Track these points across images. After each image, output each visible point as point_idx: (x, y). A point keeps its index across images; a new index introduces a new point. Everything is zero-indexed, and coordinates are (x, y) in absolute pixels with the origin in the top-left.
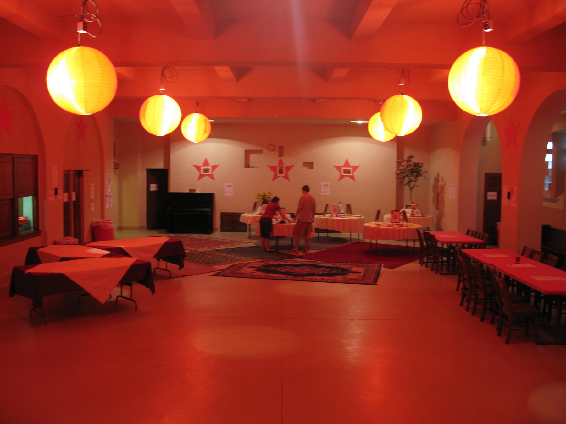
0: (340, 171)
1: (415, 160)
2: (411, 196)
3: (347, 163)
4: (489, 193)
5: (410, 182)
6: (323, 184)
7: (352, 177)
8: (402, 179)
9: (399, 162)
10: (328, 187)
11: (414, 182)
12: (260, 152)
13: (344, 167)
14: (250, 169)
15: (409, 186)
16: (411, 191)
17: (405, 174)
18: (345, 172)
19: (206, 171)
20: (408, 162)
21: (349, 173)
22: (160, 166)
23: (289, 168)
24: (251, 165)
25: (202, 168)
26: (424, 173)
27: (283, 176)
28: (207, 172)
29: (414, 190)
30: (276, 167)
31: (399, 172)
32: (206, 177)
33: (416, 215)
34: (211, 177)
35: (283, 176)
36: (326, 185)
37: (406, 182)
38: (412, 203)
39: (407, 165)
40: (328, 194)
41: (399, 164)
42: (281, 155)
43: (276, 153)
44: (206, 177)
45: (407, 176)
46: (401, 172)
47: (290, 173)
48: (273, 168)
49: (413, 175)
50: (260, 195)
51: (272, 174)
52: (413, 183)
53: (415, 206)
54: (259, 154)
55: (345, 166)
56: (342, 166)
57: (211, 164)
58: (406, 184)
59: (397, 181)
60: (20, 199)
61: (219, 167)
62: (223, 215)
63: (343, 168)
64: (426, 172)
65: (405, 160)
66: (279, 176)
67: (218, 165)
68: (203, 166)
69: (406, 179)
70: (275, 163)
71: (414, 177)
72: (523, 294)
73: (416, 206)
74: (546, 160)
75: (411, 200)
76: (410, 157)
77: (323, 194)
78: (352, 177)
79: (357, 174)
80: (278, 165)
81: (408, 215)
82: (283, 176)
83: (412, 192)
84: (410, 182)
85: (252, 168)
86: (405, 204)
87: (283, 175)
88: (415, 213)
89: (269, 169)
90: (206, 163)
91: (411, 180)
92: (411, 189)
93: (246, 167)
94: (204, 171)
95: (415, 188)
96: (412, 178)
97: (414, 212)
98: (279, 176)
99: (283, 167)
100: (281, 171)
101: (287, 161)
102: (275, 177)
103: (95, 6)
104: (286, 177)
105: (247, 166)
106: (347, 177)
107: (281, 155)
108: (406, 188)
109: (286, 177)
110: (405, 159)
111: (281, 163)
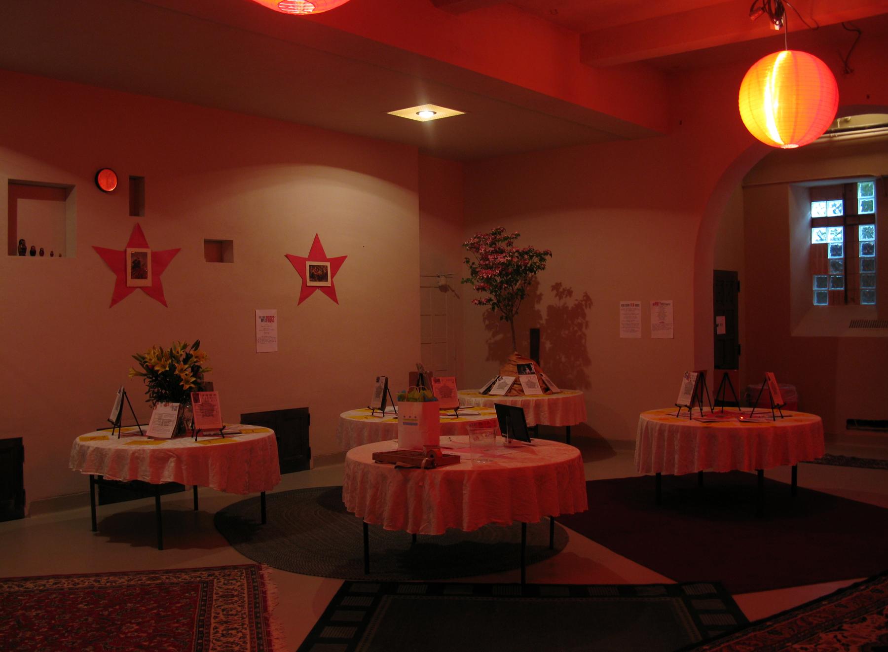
4: (718, 318)
6: (260, 313)
7: (330, 292)
10: (274, 325)
12: (62, 193)
13: (309, 259)
14: (28, 257)
18: (313, 277)
21: (324, 277)
23: (162, 260)
27: (144, 289)
32: (138, 295)
33: (527, 391)
35: (144, 289)
36: (270, 319)
40: (273, 347)
44: (318, 291)
47: (166, 278)
48: (111, 258)
51: (111, 278)
56: (306, 255)
63: (308, 263)
68: (310, 258)
70: (119, 242)
72: (53, 604)
77: (261, 348)
78: (330, 292)
79: (342, 281)
80: (130, 245)
82: (144, 289)
85: (33, 253)
87: (148, 282)
89: (97, 257)
93: (11, 252)
99: (145, 254)
100: (139, 271)
102: (121, 292)
104: (156, 292)
105: (18, 248)
107: (135, 210)
109: (156, 292)
111: (138, 237)
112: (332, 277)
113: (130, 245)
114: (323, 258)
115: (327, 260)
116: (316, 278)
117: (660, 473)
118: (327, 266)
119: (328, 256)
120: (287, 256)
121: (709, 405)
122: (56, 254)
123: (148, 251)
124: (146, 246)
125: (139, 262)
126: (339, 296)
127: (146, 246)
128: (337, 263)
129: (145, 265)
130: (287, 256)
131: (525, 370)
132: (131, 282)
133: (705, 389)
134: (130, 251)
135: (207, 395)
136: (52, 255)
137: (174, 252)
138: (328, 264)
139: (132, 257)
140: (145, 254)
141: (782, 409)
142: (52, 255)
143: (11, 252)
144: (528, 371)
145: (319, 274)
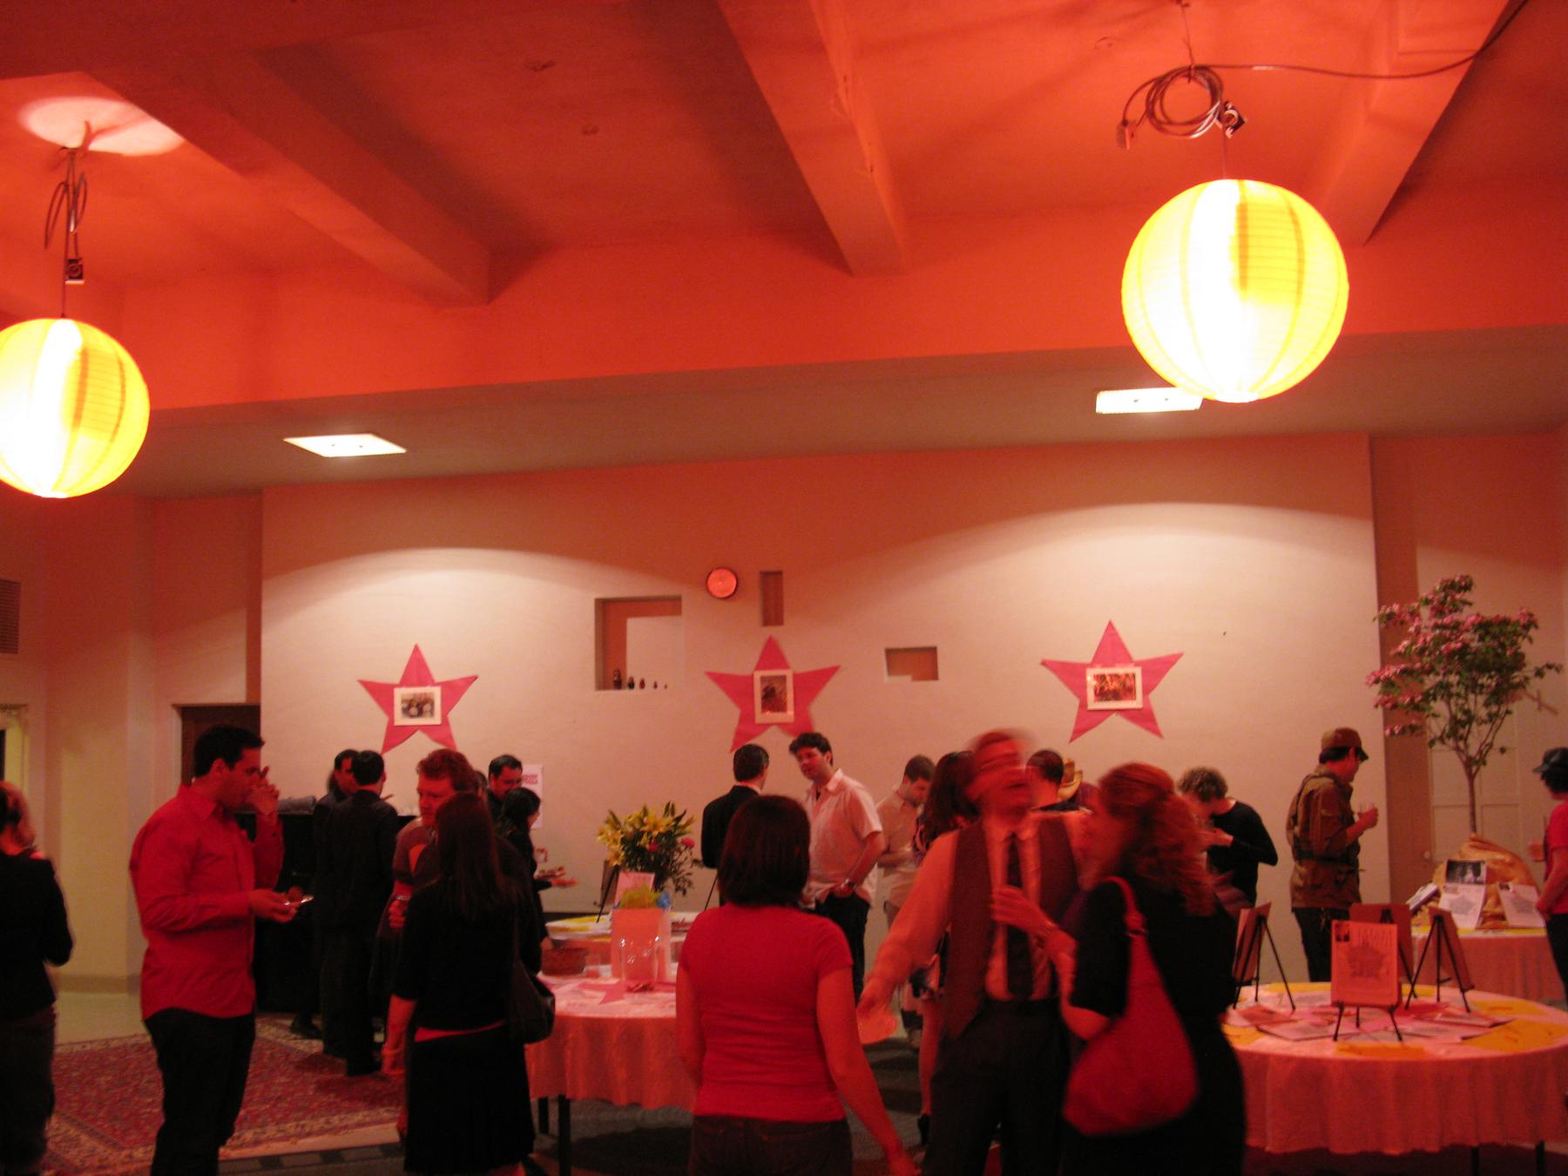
0: (1078, 688)
1: (1484, 603)
2: (1473, 805)
3: (1112, 646)
5: (1458, 728)
8: (1416, 707)
9: (1390, 616)
11: (1485, 728)
12: (666, 606)
14: (626, 692)
15: (1457, 749)
16: (1471, 777)
17: (1430, 681)
18: (1102, 694)
19: (418, 706)
20: (1439, 611)
22: (232, 692)
23: (811, 683)
24: (633, 671)
25: (400, 694)
26: (1539, 673)
28: (420, 713)
29: (1485, 774)
30: (749, 680)
31: (1392, 670)
33: (1513, 918)
34: (1145, 718)
37: (1437, 726)
38: (1483, 844)
39: (1436, 626)
41: (1391, 626)
42: (772, 615)
43: (752, 611)
44: (419, 735)
45: (1444, 690)
46: (1404, 671)
48: (735, 687)
49: (1474, 687)
50: (614, 822)
52: (1477, 736)
53: (1502, 862)
54: (664, 619)
55: (1099, 658)
56: (1087, 657)
57: (438, 677)
58: (1441, 739)
59: (1387, 722)
60: (972, 750)
61: (712, 670)
62: (1187, 785)
64: (1549, 667)
65: (1427, 602)
66: (766, 726)
67: (471, 680)
68: (405, 682)
69: (1439, 706)
70: (744, 662)
71: (1481, 699)
73: (1511, 865)
74: (712, 874)
75: (1474, 828)
76: (1450, 587)
78: (1145, 718)
79: (1165, 699)
80: (758, 667)
81: (1467, 926)
83: (1477, 780)
84: (1458, 728)
85: (631, 686)
86: (1442, 854)
87: (789, 715)
88: (1508, 908)
90: (417, 670)
91: (1467, 712)
92: (1472, 765)
93: (602, 685)
94: (406, 711)
95: (1493, 757)
96: (1477, 704)
97: (1498, 902)
98: (766, 726)
99: (783, 678)
100: (772, 699)
101: (802, 654)
103: (1271, 68)
105: (612, 676)
106: (419, 735)
107: (772, 615)
108: (1444, 764)
110: (1424, 592)
111: (772, 655)
112: (1147, 690)
113: (758, 667)
114: (1126, 658)
115: (434, 684)
116: (1110, 696)
117: (564, 1096)
118: (1134, 676)
119: (1136, 656)
120: (1044, 663)
121: (1280, 977)
122: (660, 686)
123: (758, 675)
124: (785, 665)
125: (773, 690)
126: (1161, 723)
127: (785, 665)
128: (454, 691)
129: (784, 692)
130: (1044, 663)
131: (1463, 874)
132: (761, 717)
133: (1266, 933)
134: (758, 675)
135: (639, 878)
136: (656, 686)
137: (825, 675)
138: (1138, 671)
139: (762, 683)
140: (783, 678)
141: (1399, 1015)
142: (656, 686)
143: (602, 685)
144: (1470, 876)
145: (1114, 690)
